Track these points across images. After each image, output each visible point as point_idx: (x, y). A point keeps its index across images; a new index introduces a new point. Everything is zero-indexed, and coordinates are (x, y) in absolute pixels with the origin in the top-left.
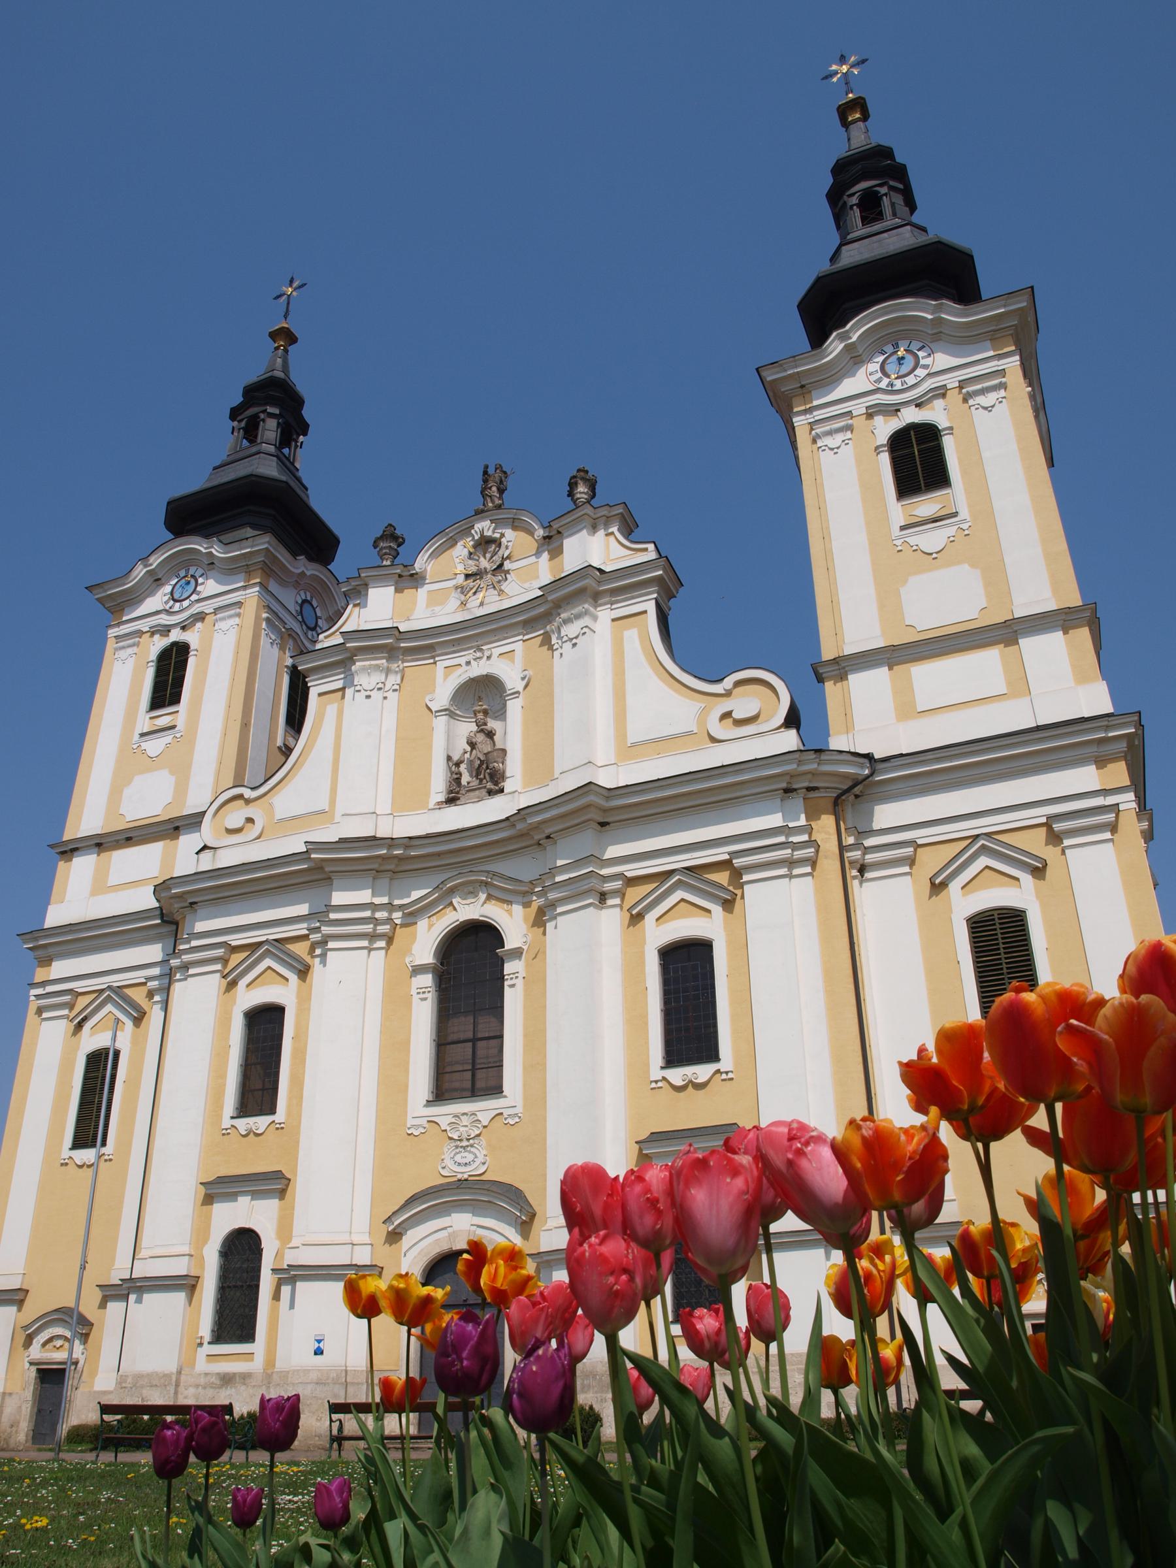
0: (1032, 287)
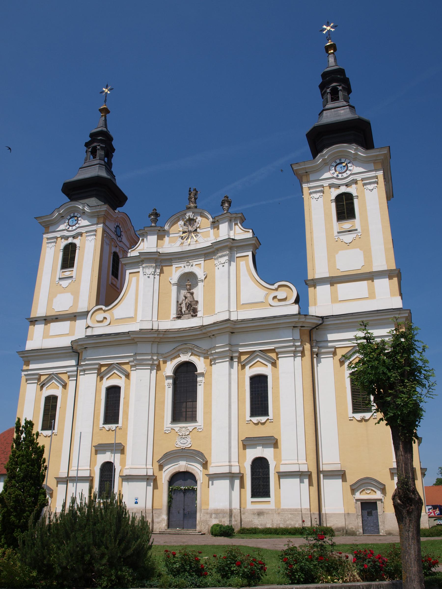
0: (389, 147)
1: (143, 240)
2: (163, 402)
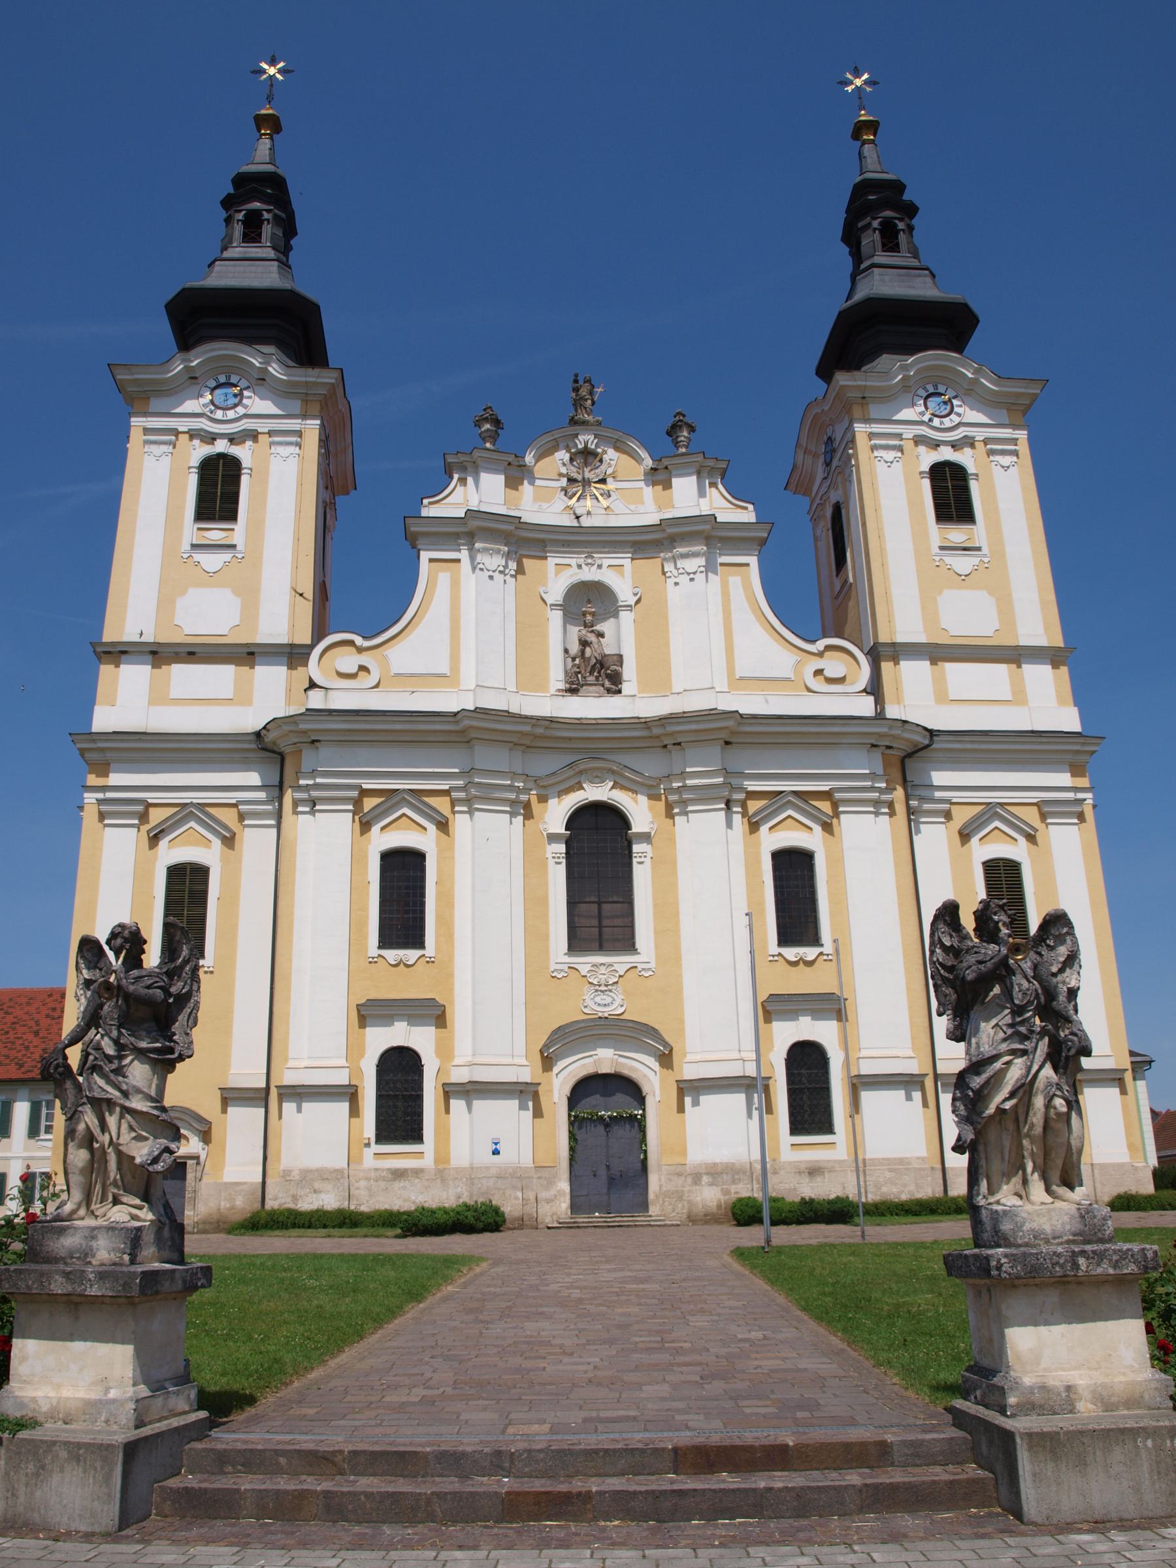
1: (463, 481)
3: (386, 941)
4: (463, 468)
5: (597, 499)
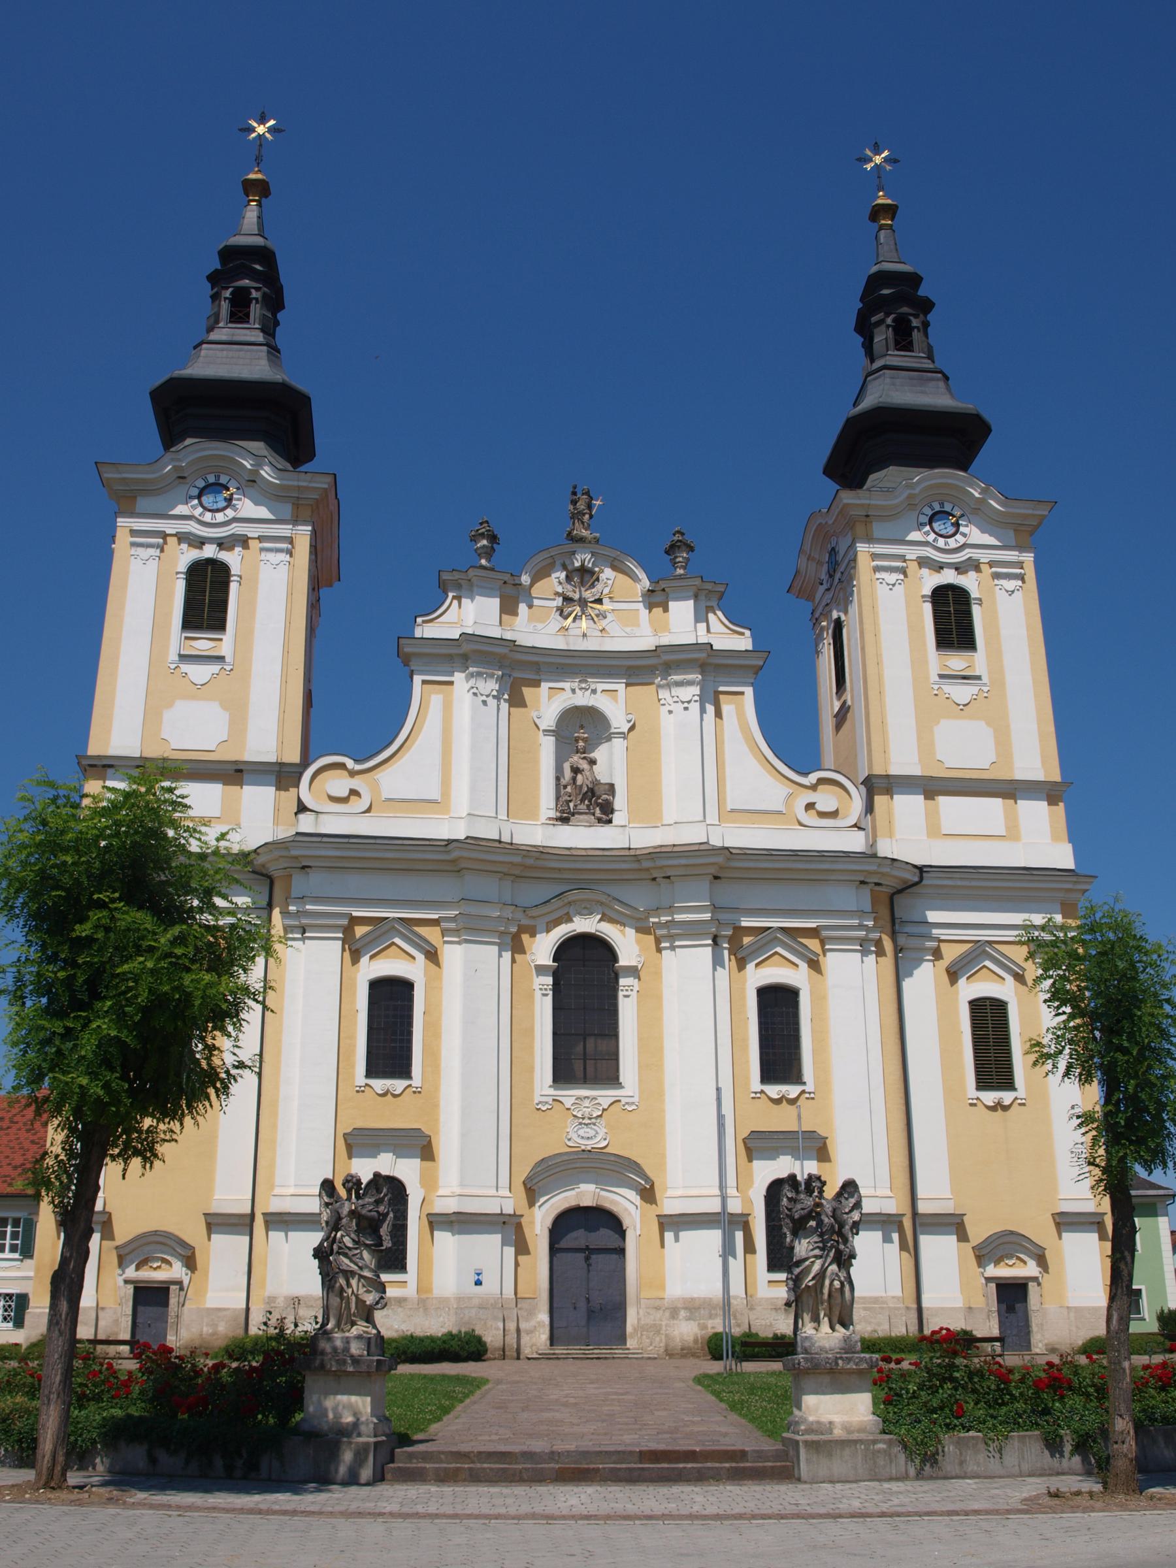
2: (530, 1032)
3: (372, 1071)
4: (458, 586)
5: (593, 619)
